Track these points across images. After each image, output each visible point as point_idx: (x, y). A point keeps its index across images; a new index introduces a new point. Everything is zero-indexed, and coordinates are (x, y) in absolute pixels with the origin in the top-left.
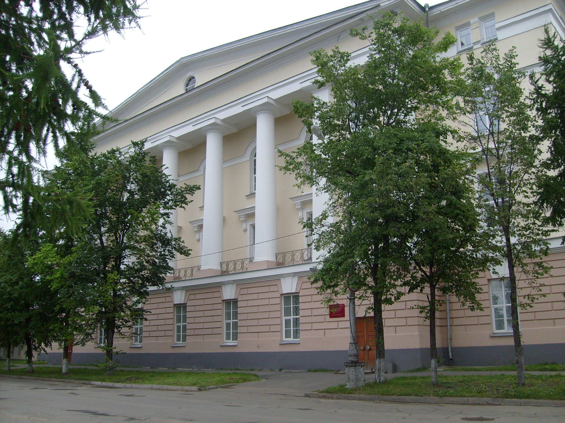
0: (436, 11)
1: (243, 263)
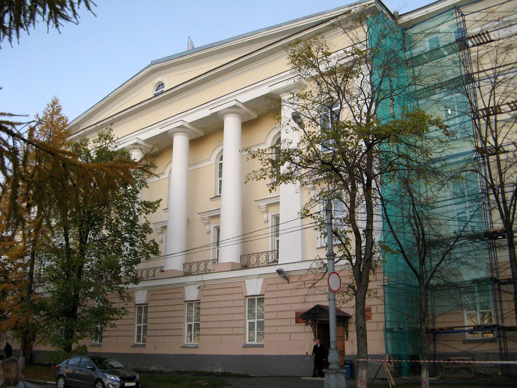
0: (405, 19)
1: (206, 265)
